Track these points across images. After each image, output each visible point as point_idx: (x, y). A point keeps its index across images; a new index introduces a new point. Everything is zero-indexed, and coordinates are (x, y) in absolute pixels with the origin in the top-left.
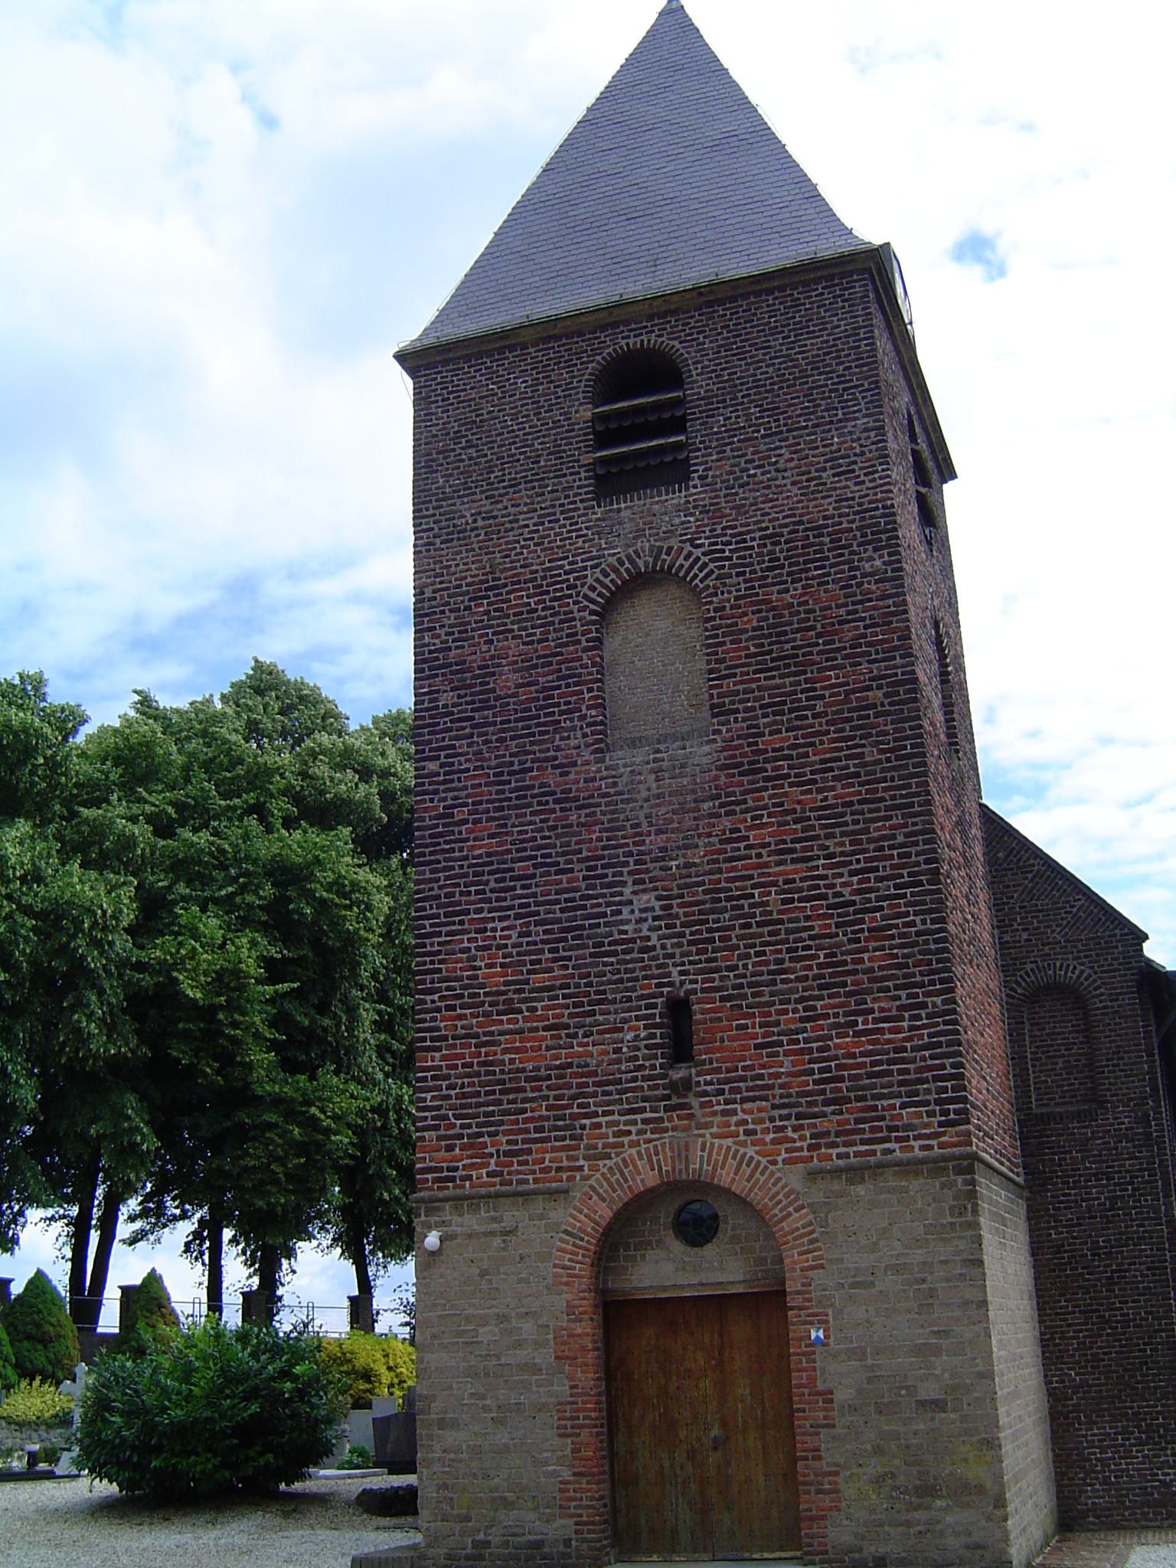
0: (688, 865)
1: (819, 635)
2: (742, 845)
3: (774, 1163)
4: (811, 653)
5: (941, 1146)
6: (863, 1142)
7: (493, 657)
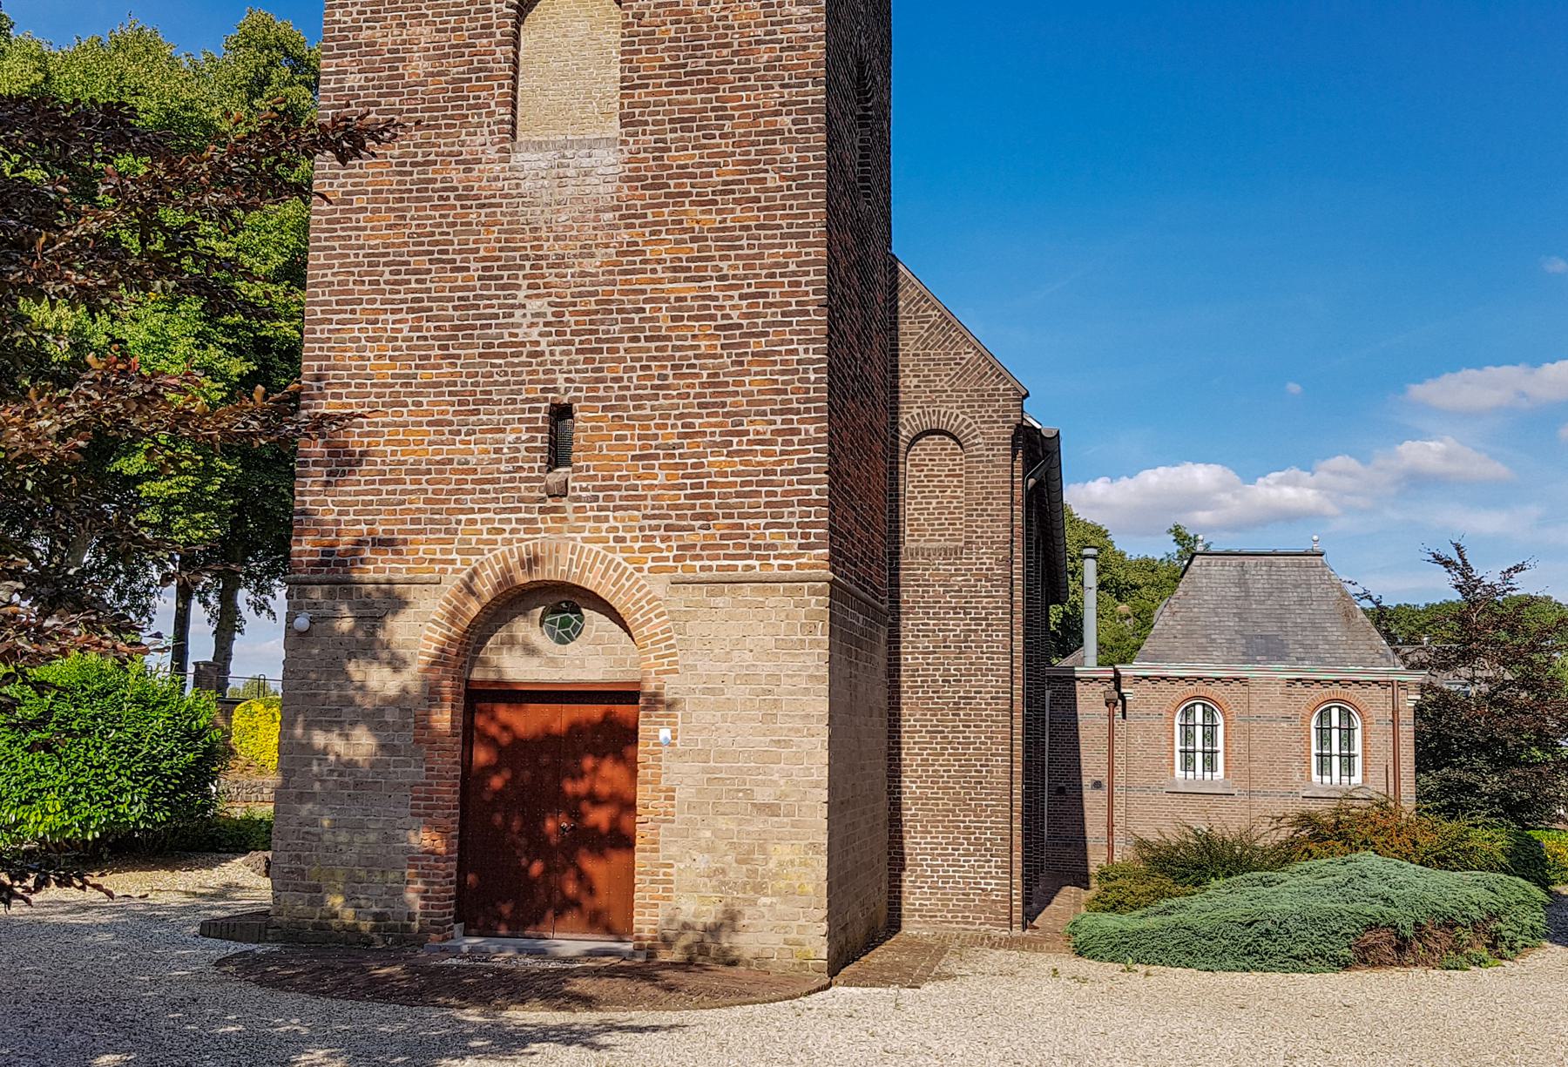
0: (583, 274)
1: (735, 53)
2: (638, 259)
3: (640, 570)
4: (725, 71)
5: (799, 566)
6: (726, 557)
7: (404, 42)
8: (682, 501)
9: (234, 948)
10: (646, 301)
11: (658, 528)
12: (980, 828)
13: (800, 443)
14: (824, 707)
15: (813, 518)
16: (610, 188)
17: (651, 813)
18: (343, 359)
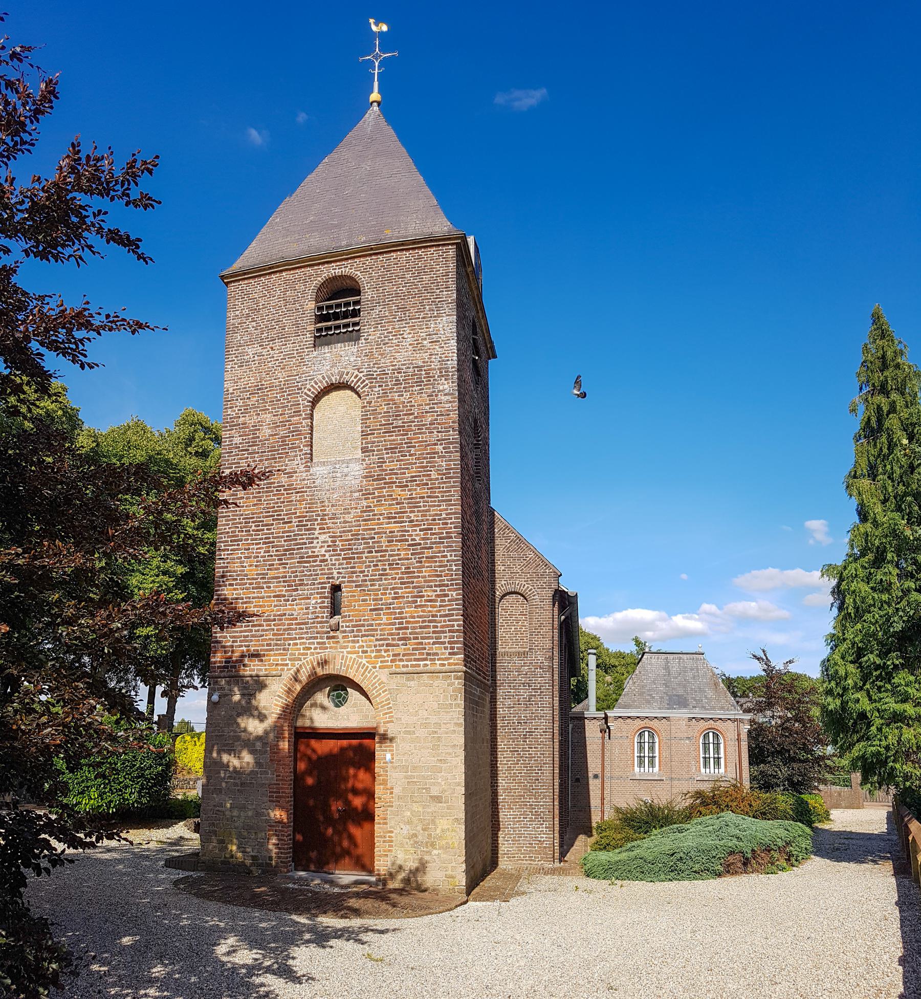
0: (345, 522)
1: (416, 417)
2: (371, 514)
3: (375, 667)
4: (411, 426)
5: (449, 664)
6: (415, 660)
7: (259, 422)
8: (394, 631)
9: (182, 874)
10: (375, 534)
11: (383, 645)
12: (538, 806)
13: (449, 601)
14: (462, 741)
15: (455, 639)
16: (358, 481)
17: (383, 802)
18: (234, 567)
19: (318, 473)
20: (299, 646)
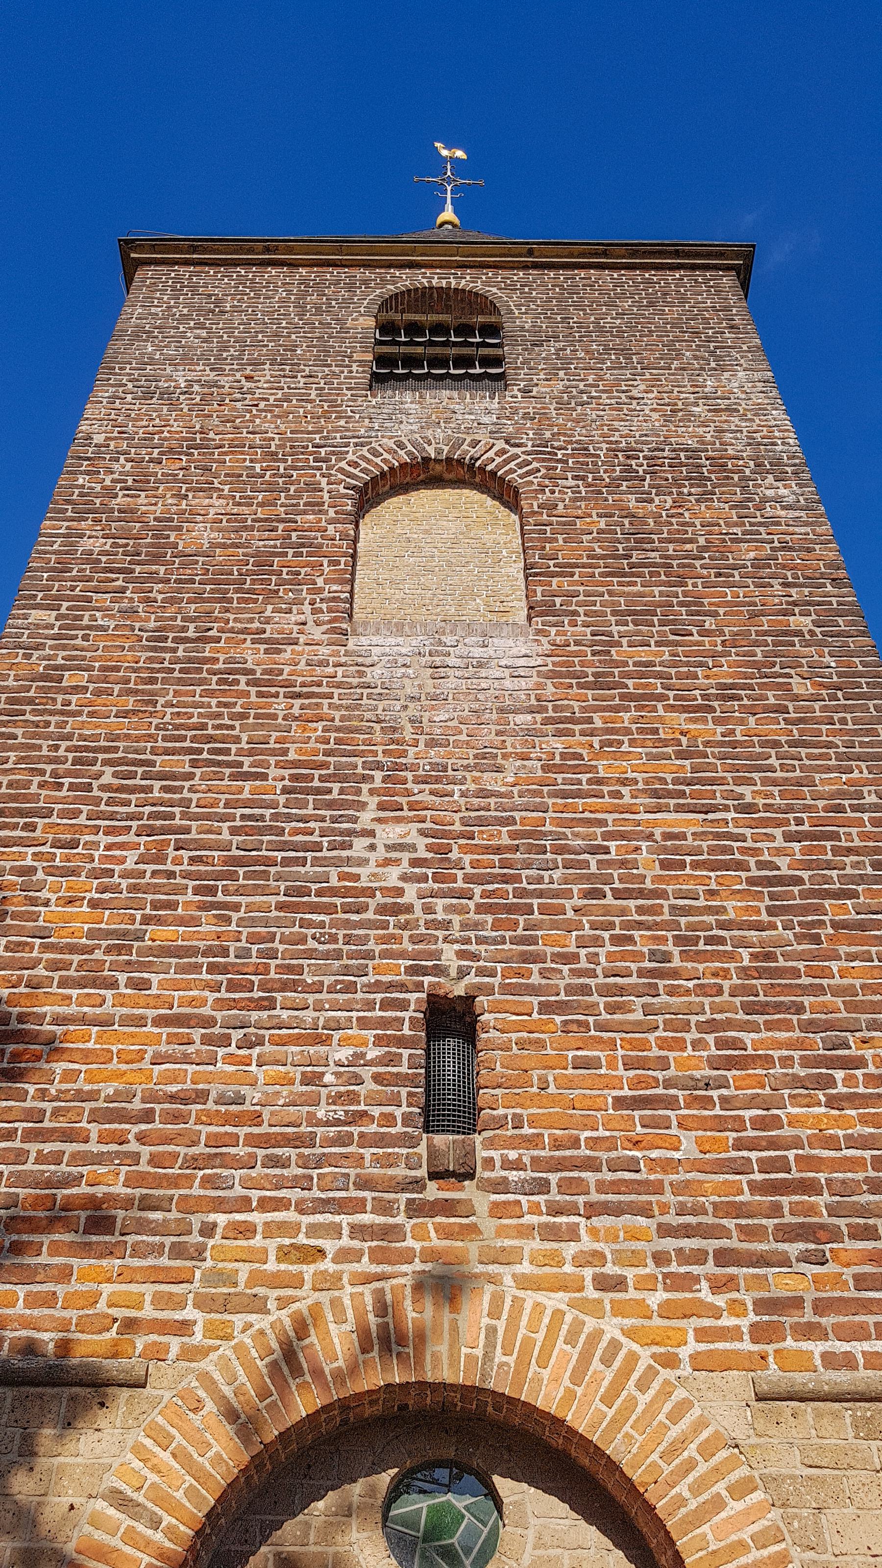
0: (484, 793)
3: (671, 1361)
8: (746, 1197)
11: (699, 1257)
19: (376, 651)
20: (258, 1241)
